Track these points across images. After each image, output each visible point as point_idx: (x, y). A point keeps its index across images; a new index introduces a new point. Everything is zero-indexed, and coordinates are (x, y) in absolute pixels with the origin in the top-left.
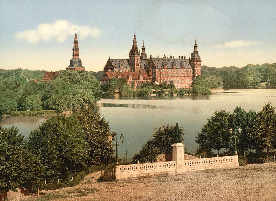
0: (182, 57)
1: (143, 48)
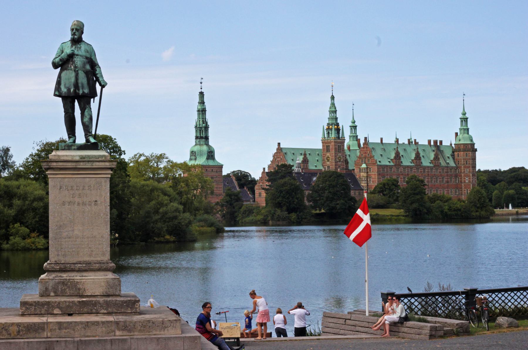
0: (436, 142)
1: (354, 125)
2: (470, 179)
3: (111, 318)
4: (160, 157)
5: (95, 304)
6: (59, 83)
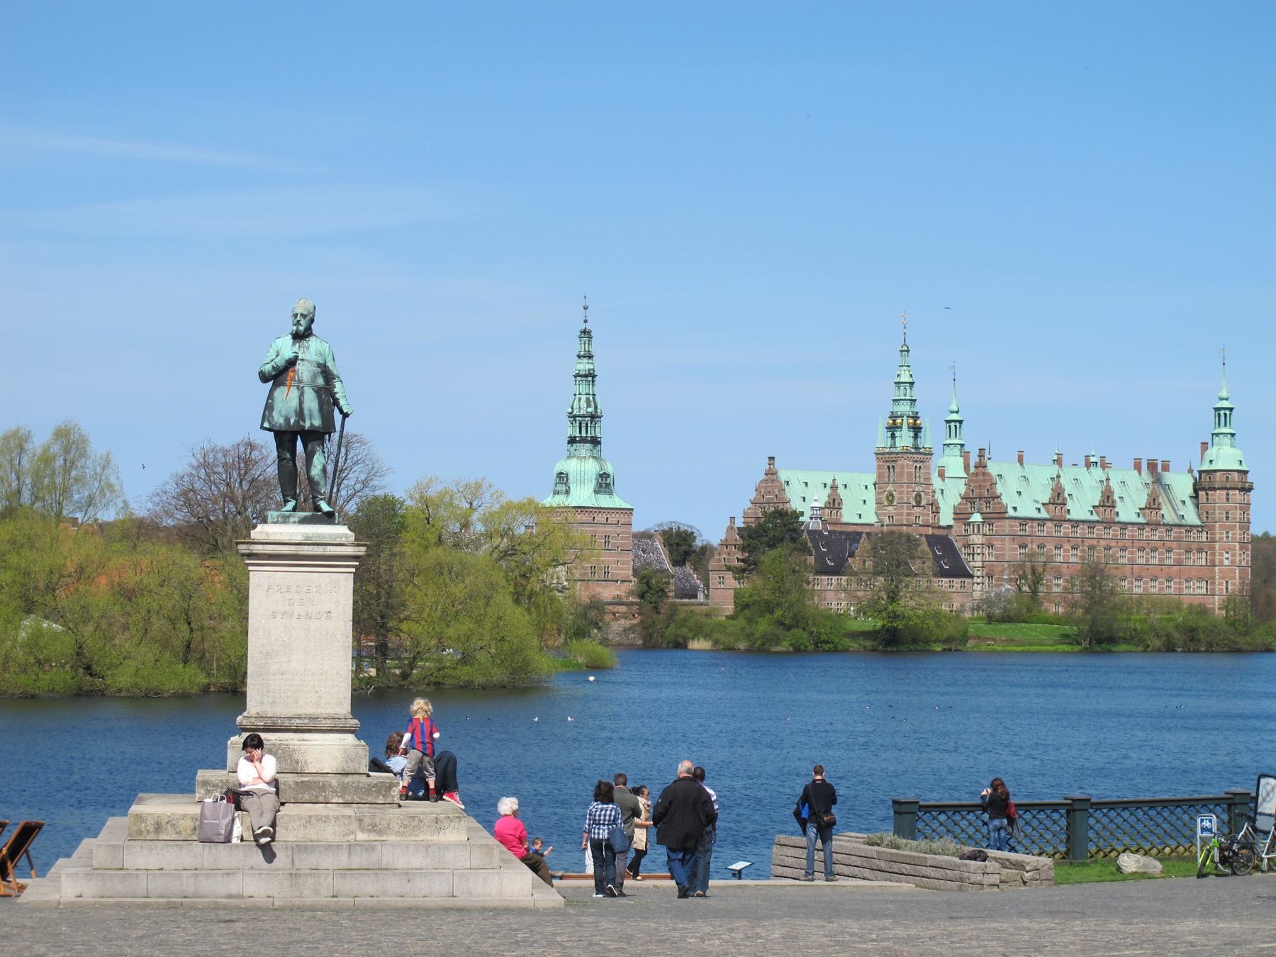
2: (1234, 555)
3: (349, 811)
4: (474, 491)
5: (323, 788)
6: (269, 407)
